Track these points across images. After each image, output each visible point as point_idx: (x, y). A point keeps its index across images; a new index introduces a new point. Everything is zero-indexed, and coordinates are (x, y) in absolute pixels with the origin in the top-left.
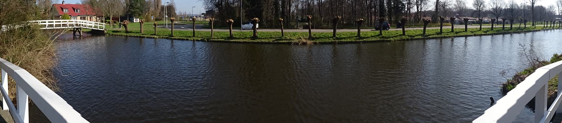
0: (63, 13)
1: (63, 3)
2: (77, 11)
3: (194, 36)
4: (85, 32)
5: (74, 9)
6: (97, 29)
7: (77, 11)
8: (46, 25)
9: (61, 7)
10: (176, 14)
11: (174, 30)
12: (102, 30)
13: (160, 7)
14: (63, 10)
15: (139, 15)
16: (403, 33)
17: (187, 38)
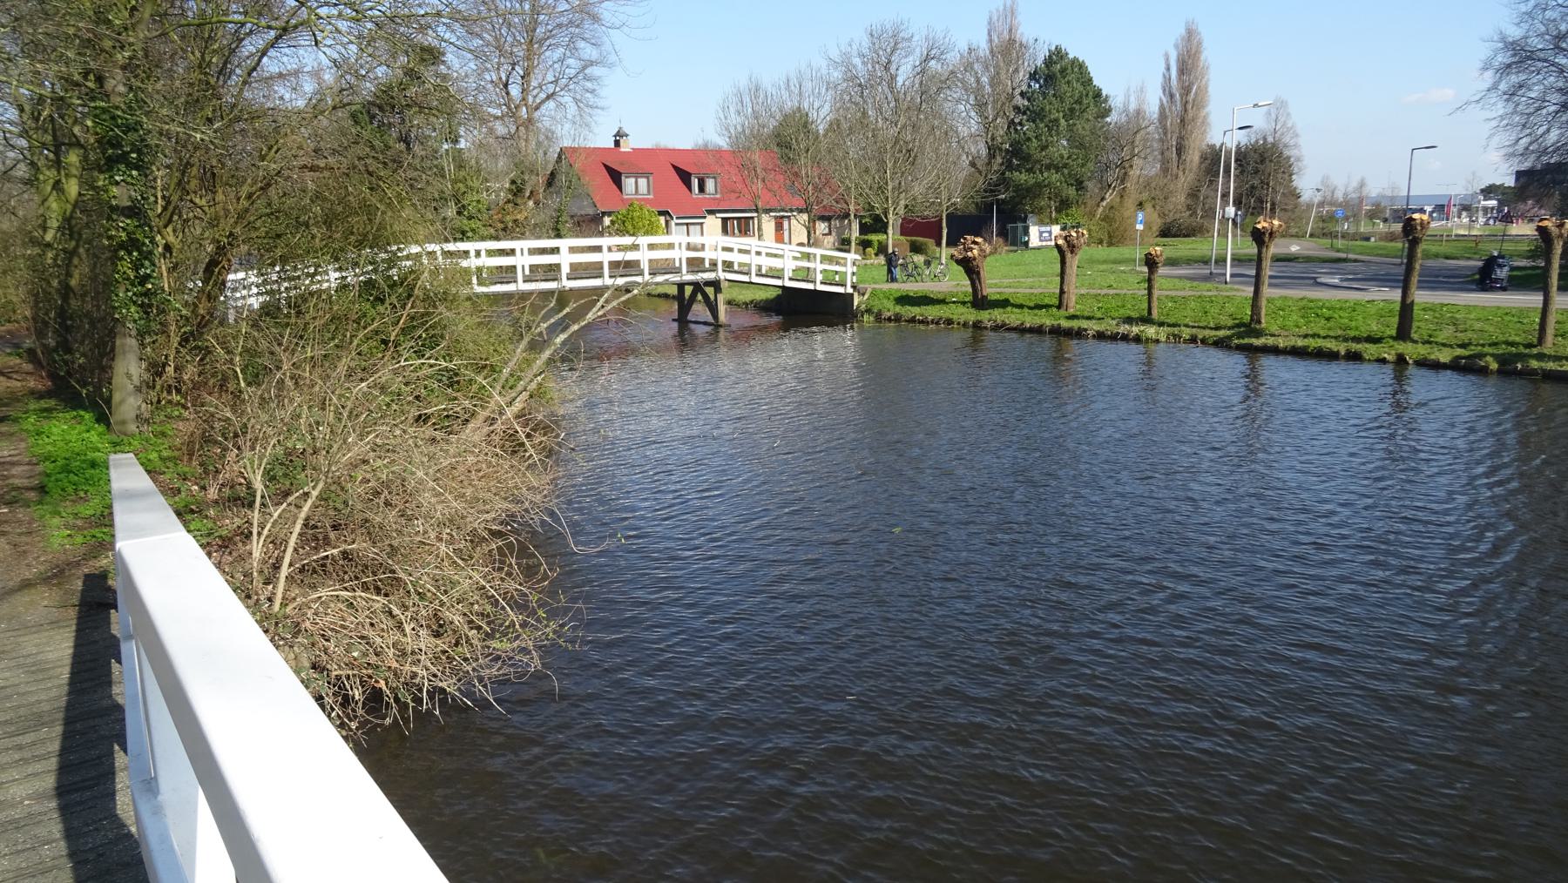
0: (623, 200)
1: (617, 143)
2: (702, 189)
3: (1403, 333)
4: (746, 304)
5: (685, 177)
6: (810, 286)
7: (702, 189)
12: (840, 290)
14: (620, 187)
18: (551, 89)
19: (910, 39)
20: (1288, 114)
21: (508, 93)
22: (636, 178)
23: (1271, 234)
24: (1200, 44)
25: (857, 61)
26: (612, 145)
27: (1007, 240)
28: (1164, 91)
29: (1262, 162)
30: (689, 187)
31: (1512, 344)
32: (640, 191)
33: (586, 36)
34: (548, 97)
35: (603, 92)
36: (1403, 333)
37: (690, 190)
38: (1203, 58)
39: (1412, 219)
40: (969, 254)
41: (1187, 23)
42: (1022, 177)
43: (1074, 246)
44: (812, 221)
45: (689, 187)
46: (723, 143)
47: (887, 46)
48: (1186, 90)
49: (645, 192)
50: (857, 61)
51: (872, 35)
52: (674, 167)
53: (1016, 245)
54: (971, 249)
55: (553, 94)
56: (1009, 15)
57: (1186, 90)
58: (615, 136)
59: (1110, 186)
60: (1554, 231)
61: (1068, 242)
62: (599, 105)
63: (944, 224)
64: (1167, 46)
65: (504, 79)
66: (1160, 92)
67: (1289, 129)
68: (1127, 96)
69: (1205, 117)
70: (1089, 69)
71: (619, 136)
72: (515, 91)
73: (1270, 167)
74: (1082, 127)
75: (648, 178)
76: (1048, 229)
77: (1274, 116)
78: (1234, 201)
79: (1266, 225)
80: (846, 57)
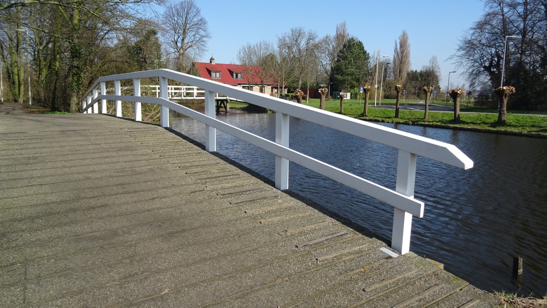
1: (211, 62)
2: (237, 77)
3: (397, 116)
4: (239, 108)
5: (231, 73)
7: (237, 77)
8: (193, 93)
9: (229, 70)
10: (440, 89)
11: (428, 111)
13: (405, 75)
14: (210, 75)
15: (353, 87)
16: (443, 263)
17: (384, 119)
18: (190, 44)
19: (304, 33)
20: (437, 61)
21: (177, 45)
22: (216, 73)
23: (368, 90)
24: (407, 38)
25: (287, 39)
26: (209, 62)
27: (332, 97)
28: (395, 52)
29: (428, 76)
30: (233, 77)
31: (429, 122)
32: (217, 77)
33: (202, 28)
34: (190, 47)
35: (207, 45)
36: (397, 116)
37: (233, 77)
38: (408, 42)
39: (396, 86)
40: (297, 94)
41: (403, 31)
42: (339, 77)
43: (323, 93)
44: (272, 88)
45: (233, 76)
46: (238, 63)
47: (297, 35)
48: (402, 52)
49: (219, 77)
50: (287, 39)
51: (292, 31)
52: (229, 70)
53: (336, 99)
54: (297, 93)
55: (191, 45)
56: (343, 26)
57: (402, 52)
58: (210, 59)
59: (367, 81)
60: (427, 90)
61: (322, 92)
62: (206, 49)
63: (308, 90)
64: (396, 38)
65: (176, 40)
66: (394, 53)
67: (437, 66)
68: (374, 54)
69: (409, 61)
70: (363, 44)
71: (212, 59)
72: (179, 45)
73: (430, 78)
74: (359, 63)
75: (219, 73)
76: (346, 94)
77: (432, 62)
78: (378, 83)
79: (366, 87)
80: (284, 37)
